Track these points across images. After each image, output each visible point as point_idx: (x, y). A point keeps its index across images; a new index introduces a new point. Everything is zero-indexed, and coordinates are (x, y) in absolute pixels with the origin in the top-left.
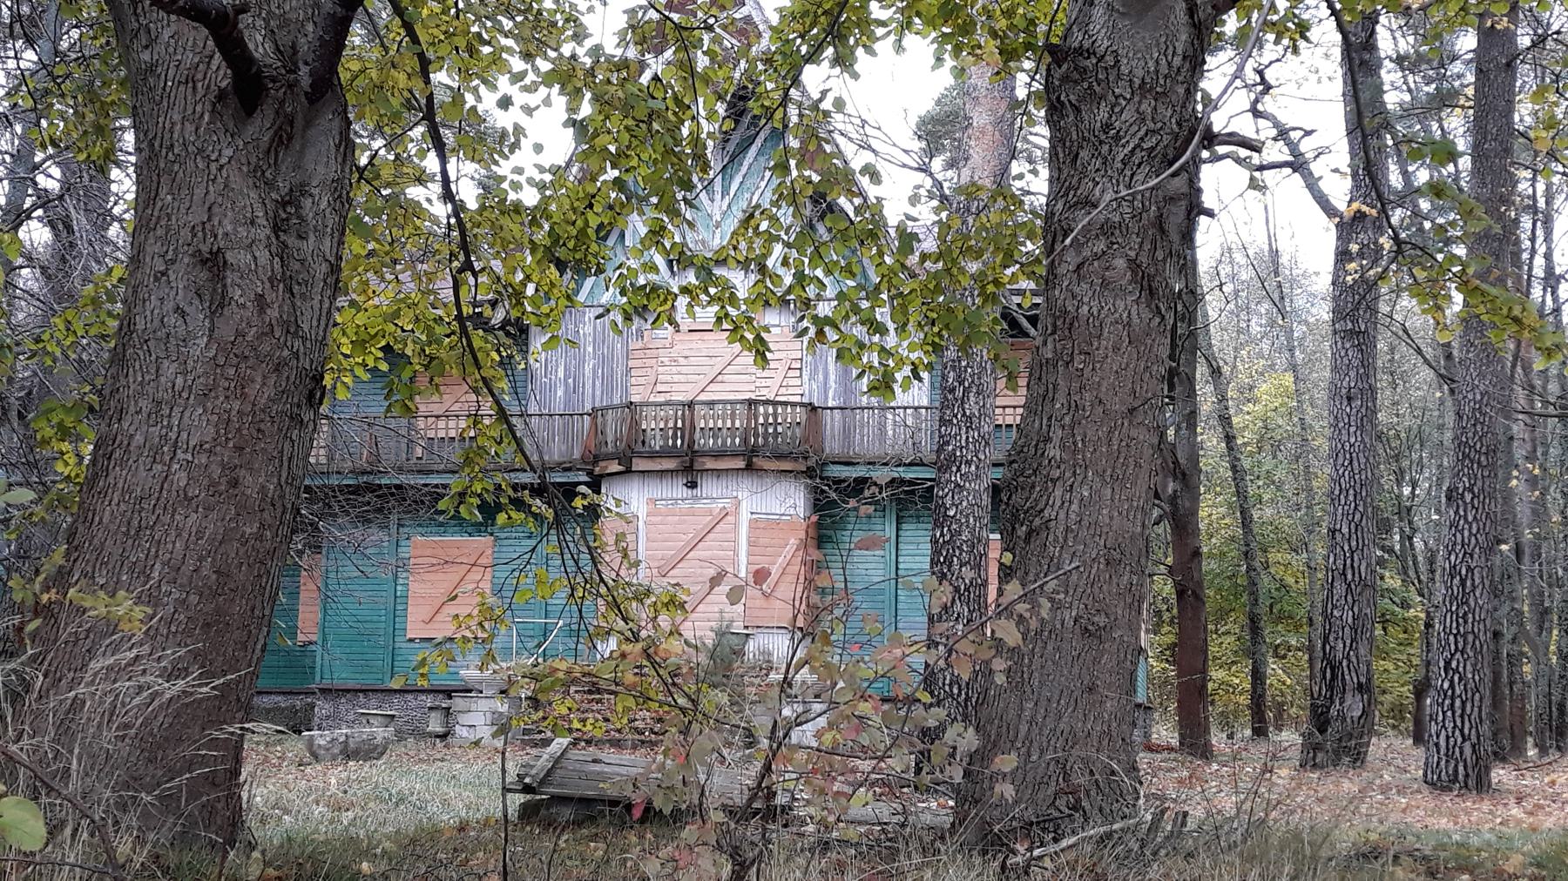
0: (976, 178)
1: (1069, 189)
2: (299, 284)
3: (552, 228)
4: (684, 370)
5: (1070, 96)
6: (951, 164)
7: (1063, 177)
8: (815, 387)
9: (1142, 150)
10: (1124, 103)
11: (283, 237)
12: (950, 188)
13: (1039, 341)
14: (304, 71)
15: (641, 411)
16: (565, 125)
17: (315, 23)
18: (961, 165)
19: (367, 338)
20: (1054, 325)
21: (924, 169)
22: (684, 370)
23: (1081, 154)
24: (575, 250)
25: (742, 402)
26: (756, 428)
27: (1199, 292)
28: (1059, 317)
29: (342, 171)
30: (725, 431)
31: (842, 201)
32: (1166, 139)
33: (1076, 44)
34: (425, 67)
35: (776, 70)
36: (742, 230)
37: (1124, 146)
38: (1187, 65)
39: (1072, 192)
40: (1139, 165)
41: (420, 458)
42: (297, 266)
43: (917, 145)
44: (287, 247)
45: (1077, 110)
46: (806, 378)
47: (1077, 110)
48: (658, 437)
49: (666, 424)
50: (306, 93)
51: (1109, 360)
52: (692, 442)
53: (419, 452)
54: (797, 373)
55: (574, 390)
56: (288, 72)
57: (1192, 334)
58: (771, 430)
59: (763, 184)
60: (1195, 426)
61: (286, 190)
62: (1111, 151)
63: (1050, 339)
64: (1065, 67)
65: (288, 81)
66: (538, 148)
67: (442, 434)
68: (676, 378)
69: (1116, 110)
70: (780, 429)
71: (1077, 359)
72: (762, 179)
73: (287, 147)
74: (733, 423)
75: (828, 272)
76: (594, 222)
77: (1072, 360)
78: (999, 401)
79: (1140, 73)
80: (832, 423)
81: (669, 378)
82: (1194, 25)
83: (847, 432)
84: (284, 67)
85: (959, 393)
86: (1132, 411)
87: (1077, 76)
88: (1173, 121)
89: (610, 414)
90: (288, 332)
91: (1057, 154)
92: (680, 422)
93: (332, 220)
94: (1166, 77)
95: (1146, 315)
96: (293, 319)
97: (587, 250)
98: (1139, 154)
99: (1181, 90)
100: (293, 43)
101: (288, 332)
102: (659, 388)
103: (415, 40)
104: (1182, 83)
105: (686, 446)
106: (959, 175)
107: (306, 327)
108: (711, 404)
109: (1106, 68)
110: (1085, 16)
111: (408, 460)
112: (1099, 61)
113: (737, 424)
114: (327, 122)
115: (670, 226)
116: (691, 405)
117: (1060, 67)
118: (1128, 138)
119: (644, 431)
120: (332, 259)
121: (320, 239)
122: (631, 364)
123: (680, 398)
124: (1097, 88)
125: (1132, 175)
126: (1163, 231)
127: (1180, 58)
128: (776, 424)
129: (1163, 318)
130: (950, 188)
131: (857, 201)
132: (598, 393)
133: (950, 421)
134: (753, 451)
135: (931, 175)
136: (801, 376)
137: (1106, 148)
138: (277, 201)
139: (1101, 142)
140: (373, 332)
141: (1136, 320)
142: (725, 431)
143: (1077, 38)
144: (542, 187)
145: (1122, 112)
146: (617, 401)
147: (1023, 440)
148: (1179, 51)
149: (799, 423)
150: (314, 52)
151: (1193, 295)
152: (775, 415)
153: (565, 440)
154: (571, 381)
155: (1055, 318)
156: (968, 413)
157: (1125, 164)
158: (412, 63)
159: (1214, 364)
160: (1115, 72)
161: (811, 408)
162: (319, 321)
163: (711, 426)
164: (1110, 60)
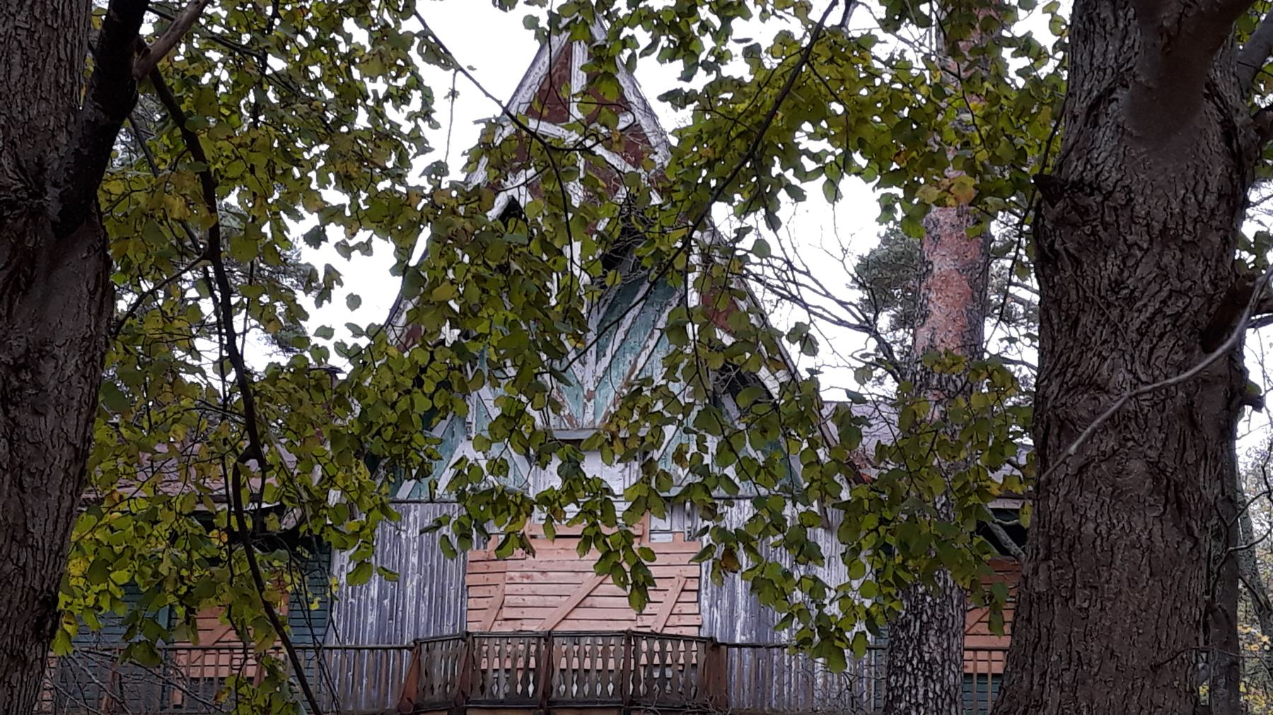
0: (938, 341)
1: (1067, 365)
2: (32, 475)
3: (363, 411)
4: (541, 589)
5: (1065, 243)
6: (901, 322)
7: (1058, 349)
8: (717, 615)
9: (1165, 316)
10: (1139, 254)
11: (13, 412)
12: (901, 352)
13: (1027, 568)
14: (52, 194)
15: (481, 645)
16: (394, 271)
17: (69, 133)
18: (917, 323)
19: (110, 558)
20: (1048, 548)
21: (868, 327)
22: (541, 589)
23: (1083, 320)
24: (393, 441)
25: (618, 634)
26: (636, 670)
27: (1239, 499)
28: (1053, 537)
29: (97, 326)
30: (594, 674)
31: (763, 373)
32: (1197, 303)
33: (1074, 177)
34: (210, 188)
35: (674, 205)
36: (626, 412)
37: (1140, 311)
38: (1223, 206)
39: (1071, 370)
40: (1161, 336)
41: (180, 707)
42: (30, 450)
43: (856, 295)
44: (17, 425)
45: (1077, 263)
46: (705, 603)
47: (1077, 263)
48: (503, 681)
49: (514, 665)
50: (54, 224)
51: (1123, 598)
52: (549, 689)
53: (178, 697)
54: (694, 597)
55: (391, 616)
56: (30, 196)
57: (1231, 557)
58: (656, 675)
59: (652, 343)
60: (1237, 682)
61: (21, 350)
62: (1122, 316)
63: (1043, 567)
64: (1060, 205)
65: (30, 207)
66: (354, 302)
67: (210, 673)
68: (529, 600)
69: (1131, 262)
70: (669, 673)
71: (1080, 594)
72: (651, 336)
73: (25, 293)
74: (605, 664)
75: (743, 472)
76: (423, 405)
77: (1073, 597)
78: (970, 642)
79: (1161, 215)
80: (742, 664)
81: (519, 600)
82: (1232, 155)
83: (760, 681)
84: (26, 189)
85: (915, 628)
86: (1155, 668)
87: (1077, 218)
88: (1206, 279)
89: (439, 650)
90: (13, 538)
91: (1049, 320)
92: (533, 661)
93: (80, 390)
94: (1195, 221)
95: (1173, 536)
96: (20, 522)
97: (409, 442)
98: (1161, 322)
99: (1216, 239)
100: (40, 158)
101: (13, 538)
102: (507, 613)
103: (199, 155)
104: (1218, 230)
105: (540, 693)
106: (914, 336)
107: (37, 532)
108: (576, 636)
109: (1115, 209)
110: (1087, 139)
111: (162, 708)
112: (1106, 199)
113: (611, 665)
114: (80, 261)
115: (529, 408)
116: (549, 637)
117: (1053, 206)
118: (1145, 300)
119: (484, 672)
120: (78, 443)
121: (61, 416)
122: (470, 580)
123: (534, 628)
124: (1102, 234)
125: (1152, 350)
126: (1194, 424)
127: (1214, 197)
128: (664, 665)
129: (1196, 541)
130: (901, 352)
131: (783, 376)
132: (423, 619)
133: (902, 668)
134: (632, 703)
135: (876, 335)
136: (698, 601)
137: (1115, 313)
138: (8, 365)
139: (1109, 305)
140: (117, 549)
141: (1159, 544)
142: (594, 674)
143: (1076, 168)
144: (353, 354)
145: (1137, 265)
146: (448, 630)
147: (1006, 704)
148: (1213, 186)
149: (695, 666)
150: (67, 170)
151: (1233, 505)
152: (663, 654)
153: (376, 683)
154: (386, 602)
155: (1050, 538)
156: (927, 657)
157: (1142, 335)
158: (193, 186)
159: (1262, 598)
160: (1127, 213)
161: (712, 645)
162: (56, 522)
163: (575, 666)
164: (1120, 197)
